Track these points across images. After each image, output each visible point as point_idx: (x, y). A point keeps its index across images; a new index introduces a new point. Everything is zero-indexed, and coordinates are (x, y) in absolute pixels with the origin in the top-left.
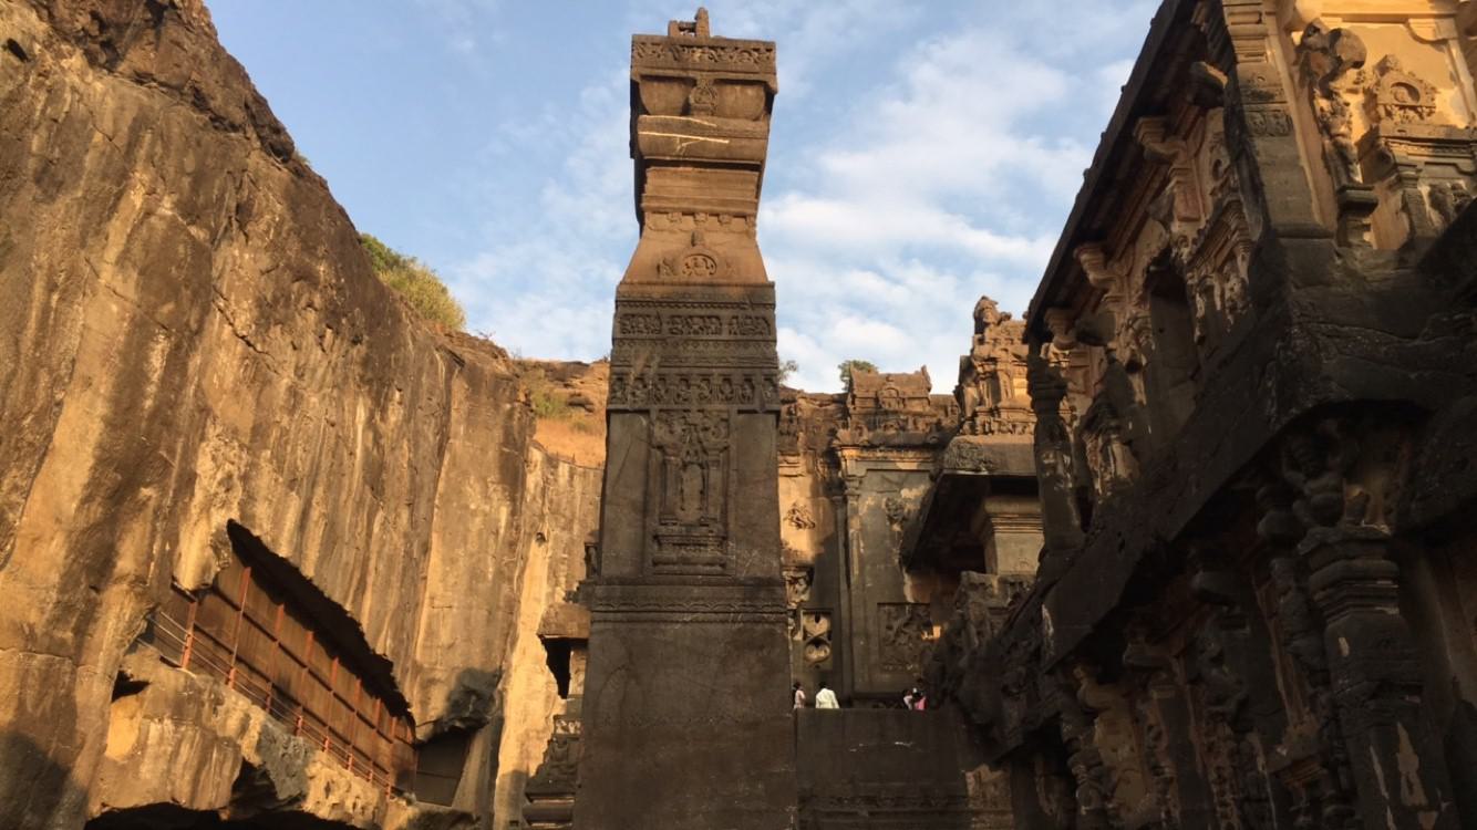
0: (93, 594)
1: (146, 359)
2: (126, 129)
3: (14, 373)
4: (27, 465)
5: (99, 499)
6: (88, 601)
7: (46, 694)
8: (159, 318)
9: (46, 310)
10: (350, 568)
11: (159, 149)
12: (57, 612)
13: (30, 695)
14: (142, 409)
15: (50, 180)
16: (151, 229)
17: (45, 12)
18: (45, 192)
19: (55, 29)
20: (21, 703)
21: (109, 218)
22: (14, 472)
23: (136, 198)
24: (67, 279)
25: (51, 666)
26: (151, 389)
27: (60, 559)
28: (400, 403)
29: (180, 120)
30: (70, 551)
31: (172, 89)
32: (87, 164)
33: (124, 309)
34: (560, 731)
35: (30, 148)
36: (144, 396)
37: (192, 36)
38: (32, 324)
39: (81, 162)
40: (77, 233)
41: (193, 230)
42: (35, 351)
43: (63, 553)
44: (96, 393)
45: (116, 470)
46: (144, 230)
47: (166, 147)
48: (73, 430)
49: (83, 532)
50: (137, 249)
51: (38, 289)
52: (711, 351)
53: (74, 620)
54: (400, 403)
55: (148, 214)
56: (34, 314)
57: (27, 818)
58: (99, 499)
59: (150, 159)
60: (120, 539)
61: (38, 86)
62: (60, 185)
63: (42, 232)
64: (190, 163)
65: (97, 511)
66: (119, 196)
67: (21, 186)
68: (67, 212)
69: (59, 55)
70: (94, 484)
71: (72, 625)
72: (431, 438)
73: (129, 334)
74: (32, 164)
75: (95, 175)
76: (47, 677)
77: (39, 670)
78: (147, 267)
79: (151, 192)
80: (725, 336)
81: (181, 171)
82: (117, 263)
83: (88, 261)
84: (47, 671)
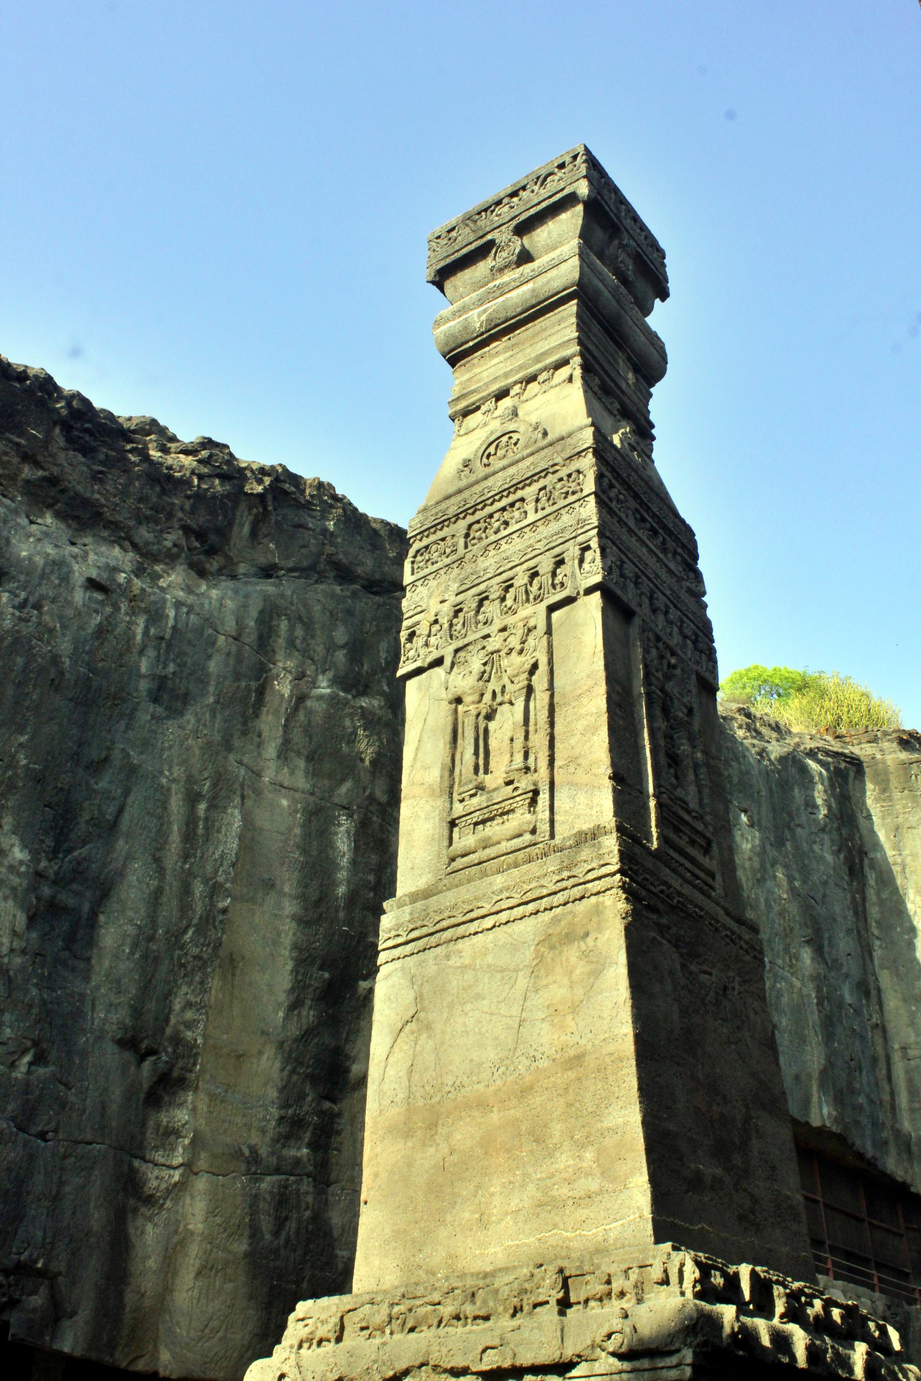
0: (327, 1105)
1: (331, 845)
2: (252, 624)
3: (158, 893)
4: (197, 978)
5: (308, 1002)
6: (321, 1113)
7: (286, 1218)
8: (336, 800)
9: (191, 821)
11: (299, 632)
12: (283, 1129)
13: (266, 1224)
14: (337, 899)
15: (170, 696)
16: (310, 713)
17: (127, 544)
18: (168, 708)
19: (142, 555)
20: (255, 1233)
21: (257, 716)
22: (184, 989)
23: (284, 687)
24: (215, 785)
25: (286, 1187)
26: (342, 875)
28: (752, 825)
29: (319, 597)
30: (287, 1060)
31: (308, 572)
32: (211, 670)
33: (295, 801)
34: (376, 1252)
35: (139, 670)
36: (335, 884)
39: (204, 669)
40: (217, 738)
41: (364, 702)
42: (185, 863)
43: (278, 1065)
44: (281, 894)
45: (321, 968)
46: (301, 716)
47: (308, 626)
48: (264, 937)
49: (297, 1040)
50: (297, 736)
51: (176, 803)
53: (308, 1135)
54: (752, 825)
55: (301, 699)
56: (175, 828)
58: (308, 1002)
60: (347, 1040)
61: (133, 612)
62: (186, 699)
63: (170, 747)
64: (341, 635)
65: (308, 1015)
66: (261, 692)
67: (134, 709)
68: (199, 721)
69: (155, 577)
70: (299, 989)
71: (307, 1140)
72: (829, 858)
73: (306, 825)
74: (144, 686)
75: (225, 678)
76: (283, 1200)
77: (271, 1193)
78: (314, 752)
79: (300, 676)
81: (331, 647)
82: (279, 757)
83: (240, 763)
84: (282, 1195)
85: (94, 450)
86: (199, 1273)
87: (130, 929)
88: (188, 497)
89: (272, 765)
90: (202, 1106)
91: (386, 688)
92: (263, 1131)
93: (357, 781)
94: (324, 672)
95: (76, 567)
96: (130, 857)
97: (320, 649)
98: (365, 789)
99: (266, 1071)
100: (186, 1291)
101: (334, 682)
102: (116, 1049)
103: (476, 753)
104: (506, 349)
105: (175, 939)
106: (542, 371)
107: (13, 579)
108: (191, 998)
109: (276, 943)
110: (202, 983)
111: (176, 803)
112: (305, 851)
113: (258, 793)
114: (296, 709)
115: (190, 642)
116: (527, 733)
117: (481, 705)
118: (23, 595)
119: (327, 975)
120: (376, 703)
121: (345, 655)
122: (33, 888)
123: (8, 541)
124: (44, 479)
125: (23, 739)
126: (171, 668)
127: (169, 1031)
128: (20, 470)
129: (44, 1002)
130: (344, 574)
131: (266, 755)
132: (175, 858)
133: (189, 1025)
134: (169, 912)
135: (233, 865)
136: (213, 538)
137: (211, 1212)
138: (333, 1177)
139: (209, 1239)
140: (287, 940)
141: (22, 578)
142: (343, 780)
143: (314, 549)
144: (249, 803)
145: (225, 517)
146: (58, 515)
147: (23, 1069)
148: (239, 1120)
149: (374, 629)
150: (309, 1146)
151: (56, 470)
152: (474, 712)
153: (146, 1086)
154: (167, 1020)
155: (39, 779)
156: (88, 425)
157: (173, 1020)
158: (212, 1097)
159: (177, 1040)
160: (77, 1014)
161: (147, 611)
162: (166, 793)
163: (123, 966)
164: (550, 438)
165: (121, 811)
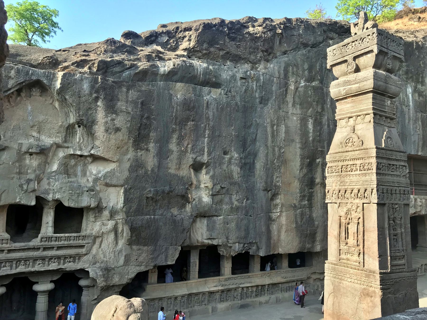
0: (311, 190)
3: (268, 153)
6: (309, 193)
8: (308, 115)
10: (417, 142)
11: (295, 69)
12: (301, 198)
13: (299, 220)
15: (264, 101)
16: (300, 91)
19: (252, 64)
20: (297, 223)
21: (286, 97)
22: (276, 174)
23: (292, 87)
27: (298, 186)
29: (299, 56)
31: (296, 49)
36: (309, 138)
37: (296, 30)
38: (270, 138)
41: (313, 84)
44: (296, 142)
46: (297, 93)
49: (303, 177)
50: (297, 99)
51: (269, 129)
52: (354, 179)
57: (307, 246)
59: (293, 73)
62: (268, 100)
64: (306, 66)
65: (305, 171)
66: (286, 90)
70: (302, 165)
74: (258, 100)
80: (358, 172)
81: (304, 71)
85: (236, 38)
86: (285, 232)
87: (262, 164)
88: (262, 42)
89: (291, 109)
90: (282, 197)
91: (319, 78)
92: (296, 200)
93: (313, 108)
94: (302, 79)
95: (237, 75)
96: (260, 146)
97: (301, 72)
98: (315, 110)
99: (296, 185)
100: (283, 236)
101: (305, 81)
102: (263, 192)
103: (345, 234)
104: (351, 102)
105: (272, 162)
106: (362, 115)
107: (223, 85)
108: (277, 175)
109: (296, 155)
110: (280, 171)
111: (269, 129)
112: (301, 130)
113: (288, 118)
114: (296, 92)
115: (267, 84)
116: (358, 235)
117: (347, 221)
118: (226, 89)
119: (308, 160)
120: (317, 83)
121: (308, 72)
122: (241, 162)
123: (220, 75)
124: (226, 53)
125: (233, 128)
126: (264, 93)
127: (273, 184)
128: (219, 54)
129: (246, 187)
130: (305, 45)
131: (289, 107)
132: (270, 143)
133: (278, 182)
134: (270, 156)
135: (284, 140)
136: (270, 51)
137: (287, 220)
138: (313, 206)
139: (287, 225)
140: (298, 154)
141: (225, 84)
142: (309, 109)
143: (296, 42)
144: (286, 121)
145: (272, 42)
146: (231, 61)
147: (245, 203)
148: (291, 198)
149: (315, 60)
150: (307, 201)
151: (228, 50)
152: (345, 223)
153: (270, 197)
154: (273, 182)
155: (237, 136)
156: (233, 31)
157: (274, 182)
158: (284, 195)
159: (276, 186)
160: (254, 186)
161: (256, 80)
162: (266, 127)
163: (262, 173)
164: (364, 146)
165: (256, 135)
